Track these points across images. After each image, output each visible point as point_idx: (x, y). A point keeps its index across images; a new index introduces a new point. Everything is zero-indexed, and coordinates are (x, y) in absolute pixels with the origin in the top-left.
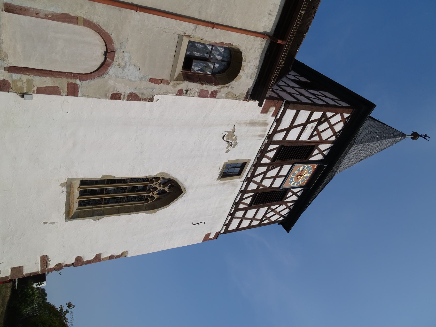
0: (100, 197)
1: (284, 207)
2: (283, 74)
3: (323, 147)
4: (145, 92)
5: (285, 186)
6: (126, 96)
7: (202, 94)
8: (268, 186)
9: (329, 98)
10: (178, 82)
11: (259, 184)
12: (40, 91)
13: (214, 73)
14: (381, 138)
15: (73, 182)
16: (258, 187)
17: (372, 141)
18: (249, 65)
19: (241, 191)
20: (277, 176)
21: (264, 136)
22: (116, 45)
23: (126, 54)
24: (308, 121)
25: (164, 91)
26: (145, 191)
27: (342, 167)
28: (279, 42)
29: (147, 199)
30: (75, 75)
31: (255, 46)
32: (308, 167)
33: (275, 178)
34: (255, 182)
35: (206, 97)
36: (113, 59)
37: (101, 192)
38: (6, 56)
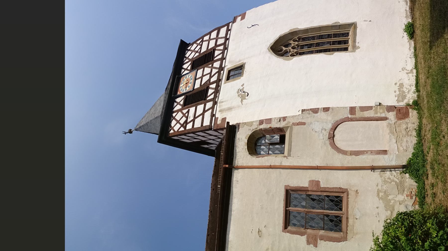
1: (190, 57)
2: (219, 147)
3: (178, 107)
4: (308, 115)
5: (194, 72)
6: (320, 110)
7: (269, 121)
8: (206, 69)
9: (186, 139)
10: (287, 126)
11: (212, 67)
12: (370, 108)
13: (264, 136)
14: (147, 124)
15: (352, 50)
16: (212, 65)
17: (151, 121)
18: (242, 147)
19: (225, 59)
20: (202, 78)
21: (220, 103)
22: (328, 142)
23: (322, 138)
24: (193, 121)
25: (295, 118)
27: (163, 99)
28: (227, 166)
30: (351, 120)
32: (183, 91)
33: (203, 76)
35: (266, 119)
36: (329, 133)
37: (334, 43)
38: (387, 126)
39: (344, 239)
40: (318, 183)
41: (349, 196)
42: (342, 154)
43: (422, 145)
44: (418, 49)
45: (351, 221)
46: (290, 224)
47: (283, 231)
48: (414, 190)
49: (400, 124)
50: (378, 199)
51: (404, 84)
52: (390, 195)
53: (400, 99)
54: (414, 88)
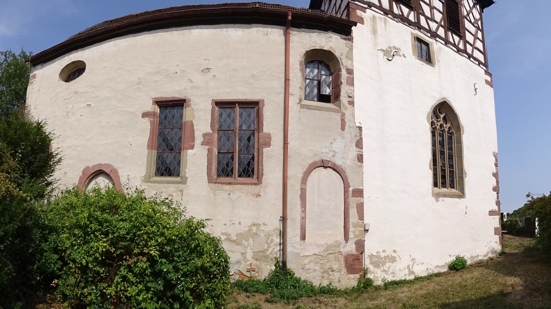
0: (447, 171)
4: (354, 134)
6: (359, 150)
7: (351, 82)
8: (441, 15)
10: (342, 105)
11: (440, 25)
12: (361, 217)
13: (331, 74)
15: (435, 192)
22: (317, 159)
23: (323, 151)
26: (443, 135)
29: (450, 133)
30: (346, 191)
31: (298, 40)
34: (437, 29)
35: (353, 78)
36: (329, 161)
37: (443, 171)
38: (337, 241)
39: (210, 181)
40: (268, 144)
41: (253, 186)
42: (303, 178)
43: (309, 296)
44: (438, 279)
45: (227, 187)
46: (222, 110)
47: (213, 100)
48: (257, 274)
49: (338, 260)
50: (249, 224)
51: (394, 264)
52: (254, 240)
53: (374, 260)
54: (390, 278)
